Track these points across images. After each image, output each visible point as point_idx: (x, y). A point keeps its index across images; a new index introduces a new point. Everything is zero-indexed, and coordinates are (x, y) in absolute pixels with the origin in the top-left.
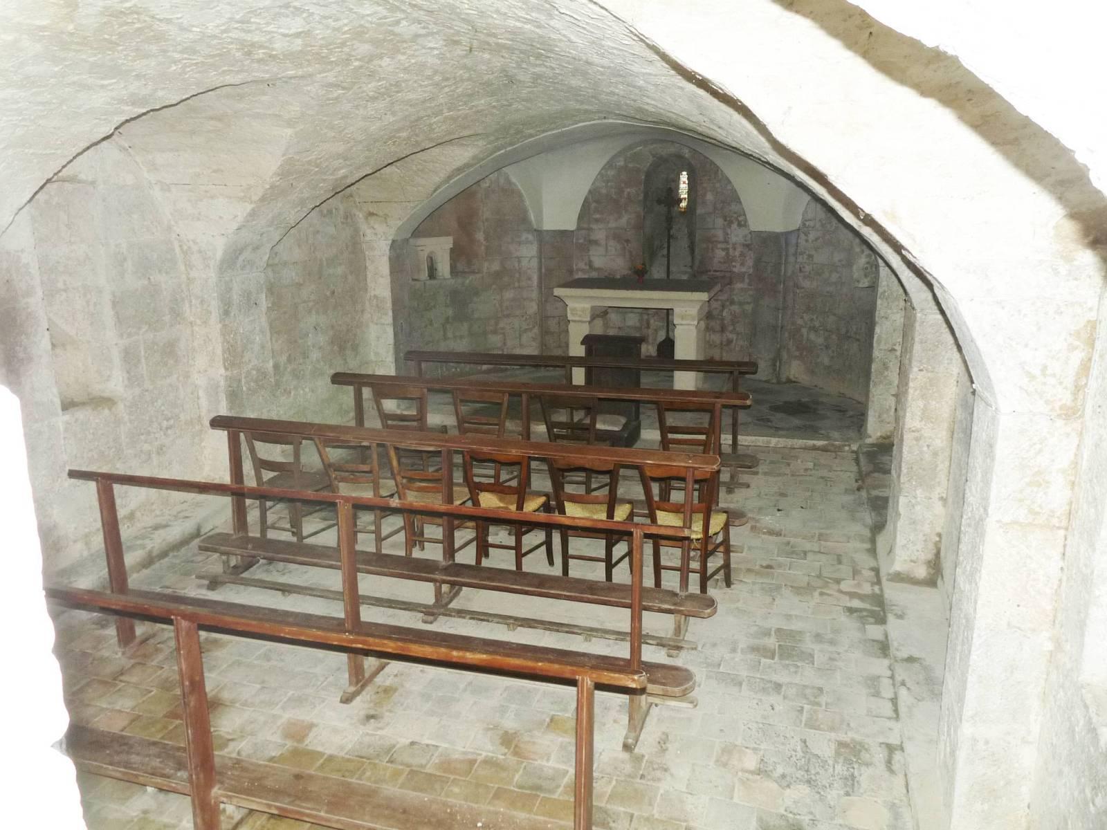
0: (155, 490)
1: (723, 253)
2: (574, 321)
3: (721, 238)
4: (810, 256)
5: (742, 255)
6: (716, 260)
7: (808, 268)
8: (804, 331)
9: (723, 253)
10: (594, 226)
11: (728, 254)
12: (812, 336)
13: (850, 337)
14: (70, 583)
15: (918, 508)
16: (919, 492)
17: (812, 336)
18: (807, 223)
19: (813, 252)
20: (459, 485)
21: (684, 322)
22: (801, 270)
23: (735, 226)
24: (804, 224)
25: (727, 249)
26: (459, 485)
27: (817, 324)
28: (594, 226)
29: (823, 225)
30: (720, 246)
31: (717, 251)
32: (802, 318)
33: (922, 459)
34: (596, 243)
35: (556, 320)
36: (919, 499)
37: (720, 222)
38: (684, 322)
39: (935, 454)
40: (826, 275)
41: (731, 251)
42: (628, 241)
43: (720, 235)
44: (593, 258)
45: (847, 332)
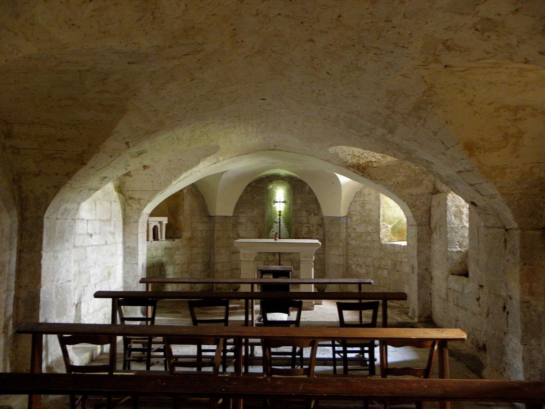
0: (86, 323)
1: (307, 229)
2: (244, 261)
3: (305, 222)
4: (354, 229)
5: (317, 229)
6: (303, 232)
7: (353, 235)
8: (353, 267)
9: (307, 229)
10: (240, 215)
11: (309, 229)
12: (358, 269)
13: (381, 268)
14: (129, 200)
15: (534, 352)
16: (533, 341)
17: (358, 269)
18: (351, 213)
19: (355, 227)
20: (102, 349)
21: (307, 260)
22: (350, 236)
23: (312, 215)
24: (350, 213)
25: (309, 227)
26: (102, 349)
27: (360, 262)
28: (240, 215)
29: (360, 213)
30: (305, 225)
31: (303, 228)
32: (352, 260)
33: (532, 320)
34: (241, 224)
35: (221, 264)
36: (533, 347)
37: (304, 213)
38: (307, 260)
39: (540, 316)
40: (364, 237)
41: (311, 228)
42: (257, 223)
43: (305, 220)
44: (239, 232)
45: (379, 265)
